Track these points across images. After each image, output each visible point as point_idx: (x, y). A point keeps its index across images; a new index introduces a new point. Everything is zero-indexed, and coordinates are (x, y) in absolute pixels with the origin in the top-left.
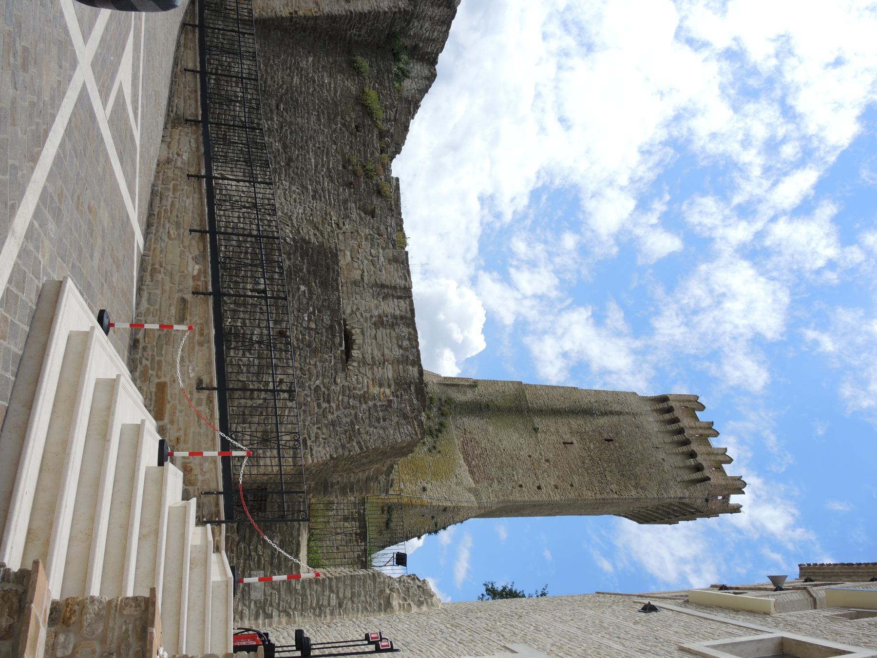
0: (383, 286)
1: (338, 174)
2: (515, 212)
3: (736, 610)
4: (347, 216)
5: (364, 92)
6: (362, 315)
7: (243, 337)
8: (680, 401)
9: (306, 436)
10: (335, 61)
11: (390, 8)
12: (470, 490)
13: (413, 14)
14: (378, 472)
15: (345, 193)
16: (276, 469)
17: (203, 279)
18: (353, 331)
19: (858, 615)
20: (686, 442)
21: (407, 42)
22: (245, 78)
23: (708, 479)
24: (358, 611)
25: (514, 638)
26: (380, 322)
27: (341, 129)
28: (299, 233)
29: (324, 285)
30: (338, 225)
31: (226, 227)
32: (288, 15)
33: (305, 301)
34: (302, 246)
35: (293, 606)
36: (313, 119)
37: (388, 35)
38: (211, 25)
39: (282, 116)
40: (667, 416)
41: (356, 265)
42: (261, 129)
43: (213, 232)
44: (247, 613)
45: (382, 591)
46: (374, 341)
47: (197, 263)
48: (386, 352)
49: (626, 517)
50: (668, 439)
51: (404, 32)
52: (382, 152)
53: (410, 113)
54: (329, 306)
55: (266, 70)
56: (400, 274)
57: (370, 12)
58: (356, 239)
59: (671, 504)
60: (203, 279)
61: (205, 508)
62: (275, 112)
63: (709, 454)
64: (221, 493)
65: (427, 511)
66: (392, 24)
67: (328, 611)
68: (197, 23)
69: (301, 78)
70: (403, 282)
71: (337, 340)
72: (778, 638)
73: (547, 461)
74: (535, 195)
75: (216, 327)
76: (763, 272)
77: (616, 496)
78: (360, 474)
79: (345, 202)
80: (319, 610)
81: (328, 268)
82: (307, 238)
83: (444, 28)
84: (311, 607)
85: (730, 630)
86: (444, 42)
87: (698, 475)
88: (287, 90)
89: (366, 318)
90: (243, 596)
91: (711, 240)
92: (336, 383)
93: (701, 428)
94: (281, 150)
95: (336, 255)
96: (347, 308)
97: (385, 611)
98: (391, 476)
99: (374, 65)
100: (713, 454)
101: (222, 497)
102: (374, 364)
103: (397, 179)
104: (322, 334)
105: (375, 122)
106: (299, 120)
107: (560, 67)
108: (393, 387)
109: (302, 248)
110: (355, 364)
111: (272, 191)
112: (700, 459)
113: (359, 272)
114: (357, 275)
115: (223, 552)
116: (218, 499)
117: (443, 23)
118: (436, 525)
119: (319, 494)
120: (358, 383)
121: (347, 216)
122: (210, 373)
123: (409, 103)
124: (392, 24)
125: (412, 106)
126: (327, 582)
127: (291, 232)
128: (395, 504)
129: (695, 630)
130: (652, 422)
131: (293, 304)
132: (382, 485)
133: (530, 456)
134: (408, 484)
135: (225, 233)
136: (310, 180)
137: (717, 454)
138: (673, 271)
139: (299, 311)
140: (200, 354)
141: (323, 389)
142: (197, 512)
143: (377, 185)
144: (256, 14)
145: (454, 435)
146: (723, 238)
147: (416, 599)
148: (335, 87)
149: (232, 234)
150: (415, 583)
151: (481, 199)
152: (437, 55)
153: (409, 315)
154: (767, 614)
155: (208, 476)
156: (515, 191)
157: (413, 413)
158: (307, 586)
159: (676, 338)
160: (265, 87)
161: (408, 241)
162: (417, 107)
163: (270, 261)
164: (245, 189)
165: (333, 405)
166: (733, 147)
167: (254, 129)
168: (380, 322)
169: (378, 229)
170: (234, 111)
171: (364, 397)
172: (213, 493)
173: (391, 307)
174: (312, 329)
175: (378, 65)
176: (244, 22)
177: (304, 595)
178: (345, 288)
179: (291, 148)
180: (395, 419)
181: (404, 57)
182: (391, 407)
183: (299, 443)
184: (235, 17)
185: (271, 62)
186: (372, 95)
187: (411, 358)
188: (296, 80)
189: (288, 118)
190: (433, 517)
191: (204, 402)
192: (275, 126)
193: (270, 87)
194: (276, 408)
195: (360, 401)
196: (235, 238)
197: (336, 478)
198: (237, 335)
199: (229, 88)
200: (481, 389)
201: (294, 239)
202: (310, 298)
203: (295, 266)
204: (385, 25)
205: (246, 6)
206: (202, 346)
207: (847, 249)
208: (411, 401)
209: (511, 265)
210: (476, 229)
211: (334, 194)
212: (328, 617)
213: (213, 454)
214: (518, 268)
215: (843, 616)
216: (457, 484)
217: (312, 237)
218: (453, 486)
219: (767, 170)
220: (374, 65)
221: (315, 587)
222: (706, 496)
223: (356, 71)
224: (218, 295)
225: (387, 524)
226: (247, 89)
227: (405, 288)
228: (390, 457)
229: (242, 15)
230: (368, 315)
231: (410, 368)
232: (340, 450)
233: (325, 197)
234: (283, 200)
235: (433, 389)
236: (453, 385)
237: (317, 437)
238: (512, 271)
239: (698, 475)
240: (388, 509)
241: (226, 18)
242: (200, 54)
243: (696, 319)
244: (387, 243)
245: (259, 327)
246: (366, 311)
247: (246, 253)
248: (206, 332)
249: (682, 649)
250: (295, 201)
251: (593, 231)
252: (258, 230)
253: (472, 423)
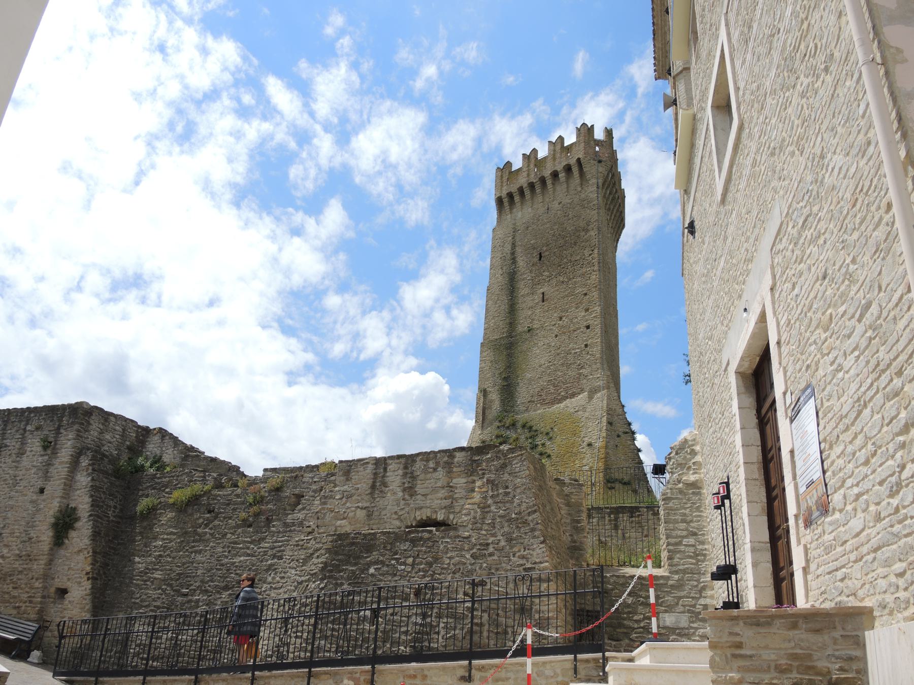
0: (373, 487)
1: (257, 532)
2: (305, 350)
3: (692, 146)
4: (301, 524)
5: (174, 504)
6: (402, 509)
7: (418, 633)
8: (502, 186)
9: (521, 568)
10: (141, 533)
11: (89, 475)
12: (590, 398)
13: (96, 451)
14: (561, 493)
15: (276, 526)
16: (553, 600)
17: (358, 675)
18: (418, 518)
19: (695, 33)
20: (543, 180)
21: (125, 456)
22: (153, 629)
23: (579, 160)
24: (700, 516)
25: (718, 361)
26: (410, 490)
27: (211, 529)
28: (315, 574)
29: (369, 549)
30: (310, 533)
31: (306, 651)
32: (90, 581)
33: (385, 569)
34: (328, 572)
35: (695, 583)
36: (199, 558)
37: (115, 477)
38: (97, 664)
39: (195, 590)
40: (517, 198)
41: (351, 515)
42: (207, 612)
43: (309, 664)
44: (702, 631)
45: (681, 491)
46: (429, 497)
47: (342, 681)
48: (439, 484)
49: (618, 240)
50: (539, 198)
51: (114, 461)
52: (236, 486)
53: (197, 456)
54: (391, 544)
55: (146, 606)
56: (362, 469)
57: (92, 496)
58: (325, 514)
59: (604, 196)
60: (358, 675)
61: (590, 673)
62: (190, 597)
63: (554, 159)
64: (575, 657)
65: (612, 443)
66: (105, 473)
67: (700, 547)
68: (93, 679)
69: (157, 570)
70: (370, 466)
71: (426, 535)
72: (712, 111)
73: (561, 318)
74: (288, 331)
75: (410, 662)
76: (362, 126)
77: (596, 251)
78: (563, 512)
79: (286, 525)
80: (699, 556)
81: (353, 544)
82: (321, 566)
83: (112, 419)
84: (696, 564)
85: (708, 154)
86: (126, 420)
87: (575, 170)
88: (167, 585)
89: (405, 504)
90: (685, 635)
91: (331, 171)
92: (469, 537)
93: (528, 166)
94: (230, 592)
95: (340, 535)
96: (393, 525)
97: (700, 488)
98: (567, 481)
99: (146, 492)
100: (554, 155)
101: (579, 656)
102: (451, 497)
103: (265, 470)
104: (419, 551)
105: (205, 493)
106: (199, 572)
107: (159, 305)
108: (474, 478)
109: (331, 571)
110: (451, 517)
111: (271, 601)
112: (559, 168)
113: (359, 512)
114: (361, 514)
115: (633, 654)
116: (582, 661)
117: (106, 420)
118: (626, 433)
119: (582, 555)
120: (469, 514)
121: (301, 524)
122: (454, 668)
123: (187, 456)
124: (105, 473)
125: (190, 454)
126: (671, 547)
127: (314, 582)
128: (605, 476)
129: (708, 187)
130: (523, 214)
131: (388, 581)
132: (573, 490)
133: (556, 336)
134: (585, 462)
135: (312, 652)
136: (262, 561)
137: (554, 151)
138: (360, 205)
139: (395, 575)
140: (434, 679)
141: (474, 550)
142: (594, 682)
143: (270, 491)
144: (87, 616)
145: (538, 415)
146: (331, 159)
147: (688, 456)
148: (168, 534)
149: (313, 644)
150: (674, 458)
151: (290, 384)
152: (139, 427)
153: (403, 460)
154: (694, 117)
155: (558, 671)
156: (281, 351)
157: (500, 459)
158: (674, 569)
159: (426, 205)
160: (163, 607)
161: (329, 460)
162: (192, 449)
163: (342, 605)
164: (267, 631)
165: (491, 540)
166: (242, 149)
167: (206, 619)
168: (410, 490)
169: (315, 491)
170: (186, 641)
171: (484, 508)
172: (575, 665)
173: (395, 477)
174: (414, 561)
175: (147, 488)
176: (95, 629)
177: (684, 572)
178: (374, 527)
179: (228, 582)
180: (506, 477)
181: (140, 461)
182: (494, 480)
183: (526, 576)
184: (89, 638)
185: (137, 601)
186: (178, 495)
187: (446, 459)
188: (158, 575)
189: (197, 584)
190: (618, 436)
191: (483, 674)
192: (205, 598)
193: (164, 603)
194: (490, 600)
195: (487, 512)
196: (317, 643)
197: (566, 538)
198: (415, 640)
199: (163, 646)
200: (488, 385)
201: (322, 580)
202: (382, 563)
203: (349, 578)
204: (106, 480)
205: (79, 627)
206: (426, 676)
207: (339, 52)
208: (488, 460)
209: (357, 358)
210: (321, 390)
211: (278, 537)
212: (706, 547)
213: (529, 662)
214: (360, 351)
215: (695, 45)
216: (586, 411)
217: (320, 560)
218: (587, 414)
219: (265, 118)
220: (146, 492)
221: (676, 560)
222: (595, 162)
223: (152, 511)
224: (375, 660)
225: (625, 484)
226: (164, 627)
227: (375, 464)
228: (544, 482)
229: (88, 631)
230: (402, 502)
231: (456, 460)
232: (537, 533)
233: (280, 547)
234: (281, 591)
235: (489, 434)
236: (484, 413)
237: (523, 557)
238: (363, 357)
239: (575, 170)
240: (610, 482)
241: (90, 648)
242: (127, 676)
243: (407, 188)
244: (330, 482)
245: (409, 617)
246: (398, 505)
247: (333, 630)
248: (412, 672)
249: (723, 201)
250: (283, 577)
251: (323, 278)
252: (310, 617)
253: (523, 394)
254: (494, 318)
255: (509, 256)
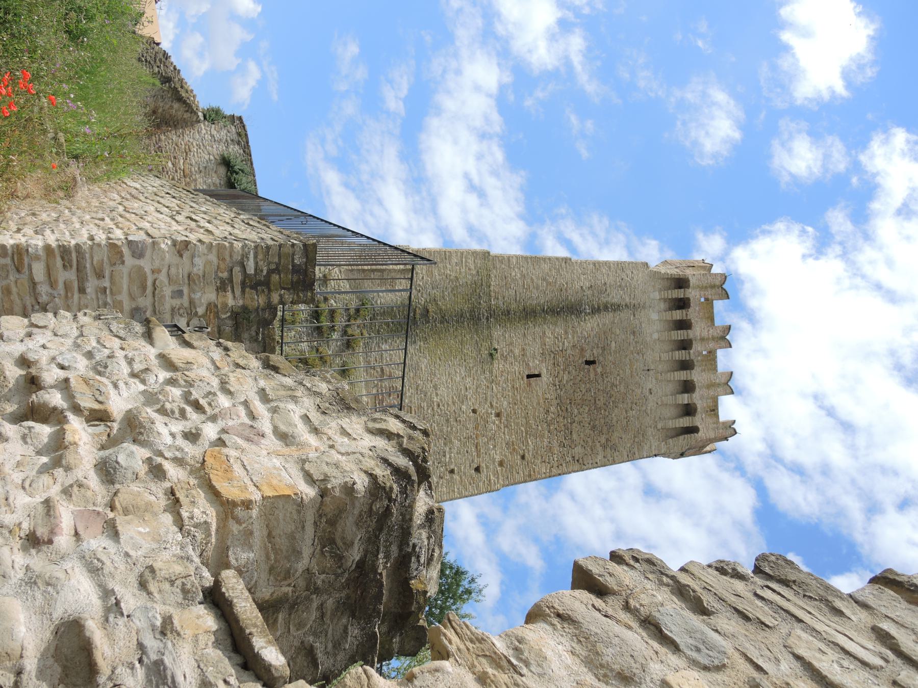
87: (685, 422)
133: (474, 411)
254: (523, 276)
255: (604, 299)
